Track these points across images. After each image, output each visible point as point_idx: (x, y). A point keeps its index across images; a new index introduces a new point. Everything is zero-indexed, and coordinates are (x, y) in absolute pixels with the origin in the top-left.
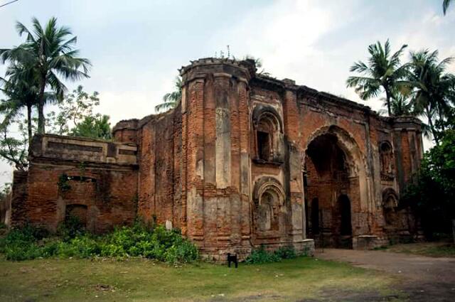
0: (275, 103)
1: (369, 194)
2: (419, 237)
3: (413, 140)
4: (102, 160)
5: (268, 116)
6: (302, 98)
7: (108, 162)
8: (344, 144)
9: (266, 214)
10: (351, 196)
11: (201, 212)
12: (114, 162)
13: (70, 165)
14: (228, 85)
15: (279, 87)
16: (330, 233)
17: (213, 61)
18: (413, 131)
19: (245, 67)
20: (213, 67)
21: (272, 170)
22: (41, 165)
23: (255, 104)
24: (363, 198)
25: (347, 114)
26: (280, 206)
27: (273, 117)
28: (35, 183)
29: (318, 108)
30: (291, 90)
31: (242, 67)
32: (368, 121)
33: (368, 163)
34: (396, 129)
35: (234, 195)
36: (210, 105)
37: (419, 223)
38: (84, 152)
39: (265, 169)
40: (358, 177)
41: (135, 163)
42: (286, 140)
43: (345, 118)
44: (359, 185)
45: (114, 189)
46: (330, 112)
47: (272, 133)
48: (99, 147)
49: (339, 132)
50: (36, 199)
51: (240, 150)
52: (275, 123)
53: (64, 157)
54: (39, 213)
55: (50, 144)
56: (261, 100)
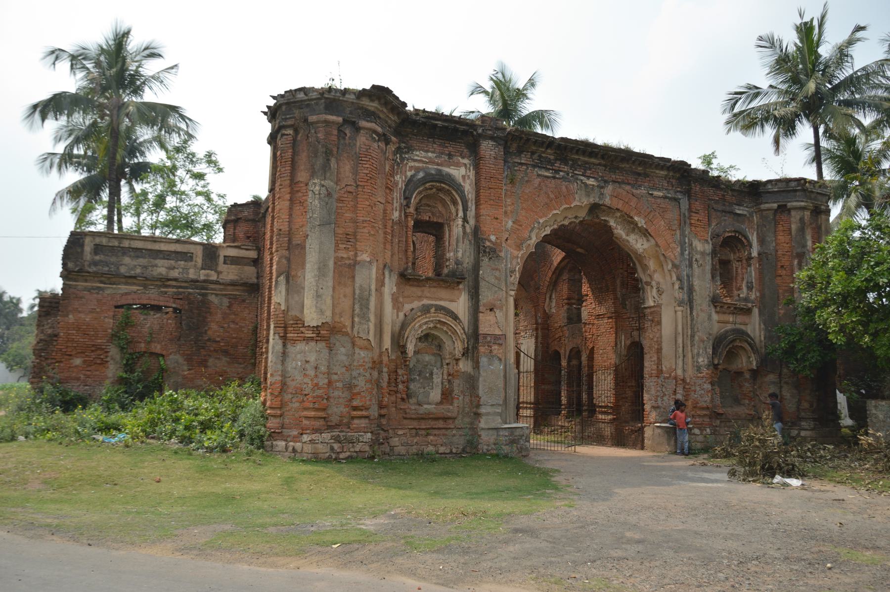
0: (458, 165)
1: (680, 341)
2: (803, 433)
3: (802, 230)
4: (192, 275)
5: (440, 190)
6: (520, 152)
7: (202, 278)
8: (628, 241)
9: (431, 374)
10: (646, 343)
11: (280, 367)
12: (214, 277)
13: (134, 284)
14: (334, 138)
15: (465, 133)
16: (610, 417)
17: (306, 94)
18: (803, 208)
19: (372, 101)
20: (308, 106)
21: (443, 293)
22: (81, 284)
23: (411, 168)
24: (667, 349)
25: (631, 179)
26: (457, 360)
27: (449, 193)
28: (71, 316)
29: (557, 171)
30: (492, 138)
32: (688, 193)
33: (678, 279)
34: (763, 206)
35: (338, 337)
37: (805, 405)
38: (160, 262)
39: (427, 291)
41: (255, 281)
42: (477, 238)
43: (628, 188)
44: (659, 323)
45: (214, 326)
46: (588, 177)
47: (450, 220)
48: (186, 253)
49: (612, 217)
50: (73, 340)
51: (356, 255)
52: (455, 203)
53: (123, 270)
54: (76, 366)
55: (98, 249)
56: (423, 159)
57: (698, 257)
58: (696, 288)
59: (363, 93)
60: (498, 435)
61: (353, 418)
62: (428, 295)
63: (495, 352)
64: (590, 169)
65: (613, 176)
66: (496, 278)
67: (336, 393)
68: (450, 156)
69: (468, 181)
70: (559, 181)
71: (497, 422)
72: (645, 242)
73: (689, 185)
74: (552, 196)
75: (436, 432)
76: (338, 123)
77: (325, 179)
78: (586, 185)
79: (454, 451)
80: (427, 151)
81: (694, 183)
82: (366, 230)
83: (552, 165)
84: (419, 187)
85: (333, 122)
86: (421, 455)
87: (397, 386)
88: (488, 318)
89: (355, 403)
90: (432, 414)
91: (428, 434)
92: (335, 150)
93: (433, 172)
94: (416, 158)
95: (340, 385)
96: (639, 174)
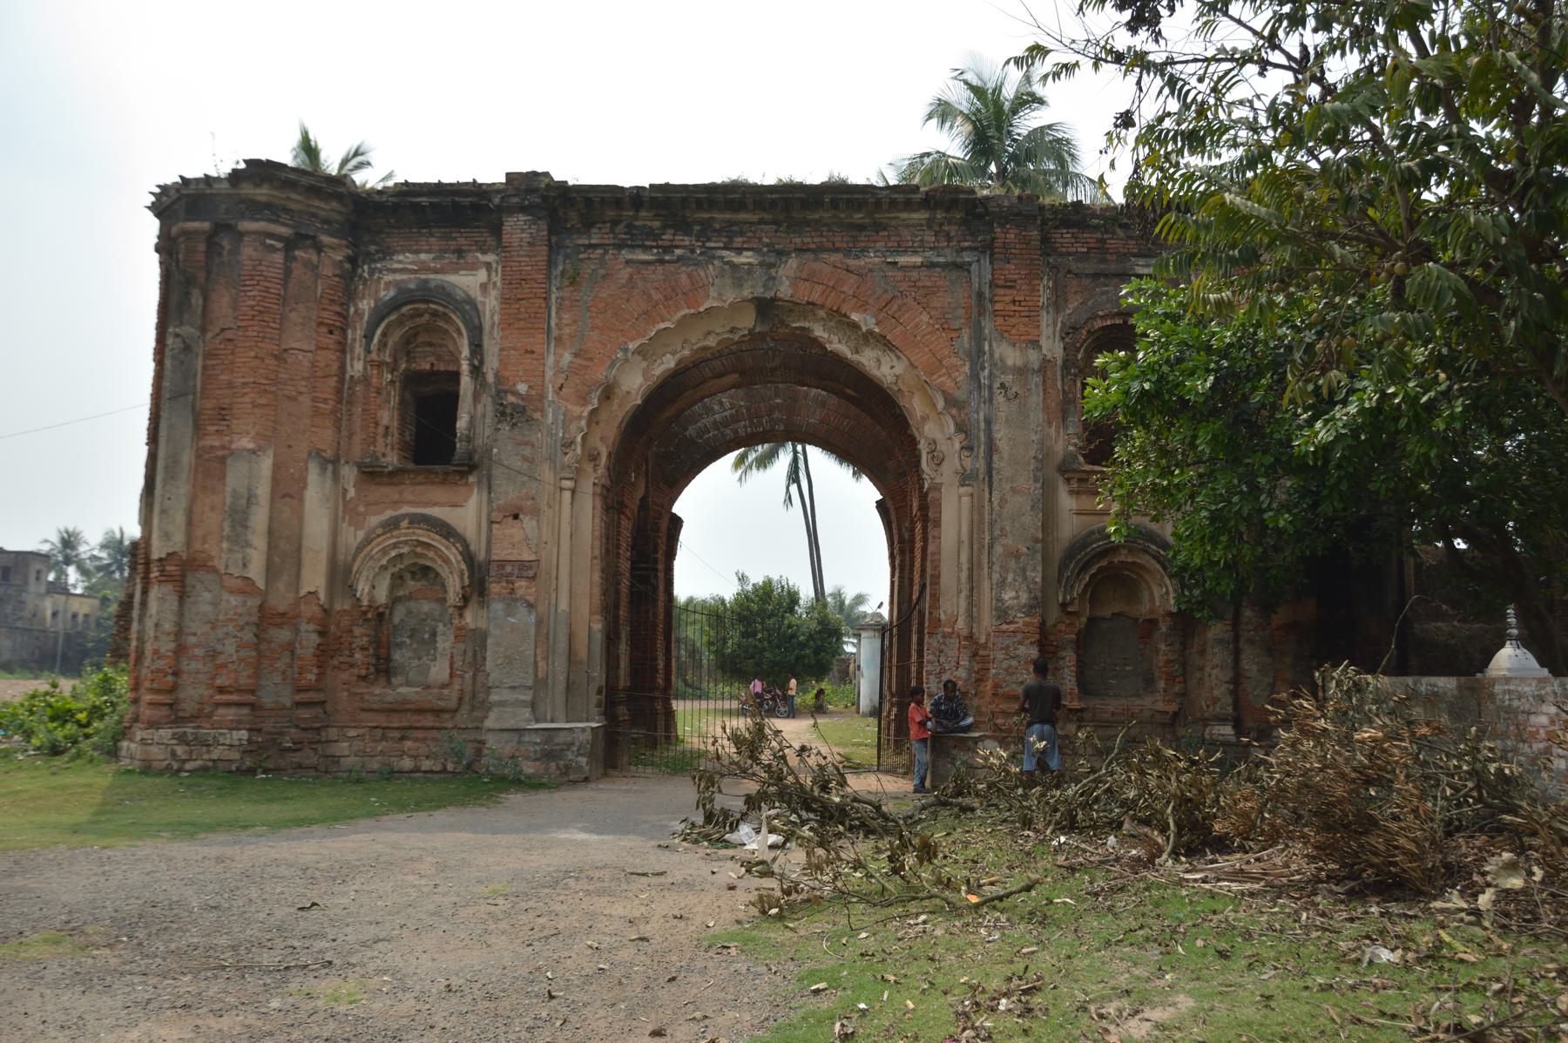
0: (473, 267)
5: (435, 314)
9: (434, 634)
14: (201, 257)
21: (438, 493)
23: (388, 284)
29: (668, 249)
30: (522, 209)
31: (247, 190)
32: (988, 248)
35: (201, 574)
43: (836, 258)
46: (739, 251)
49: (817, 320)
56: (405, 266)
57: (1008, 379)
58: (1002, 445)
59: (235, 175)
60: (519, 742)
61: (218, 705)
62: (411, 498)
63: (520, 592)
64: (742, 234)
65: (798, 240)
66: (525, 458)
67: (193, 665)
68: (460, 253)
69: (494, 293)
70: (672, 268)
71: (523, 718)
72: (895, 362)
73: (992, 231)
74: (656, 296)
75: (420, 734)
76: (204, 232)
77: (181, 324)
78: (734, 267)
79: (450, 767)
80: (417, 252)
81: (1002, 226)
82: (247, 399)
83: (657, 237)
84: (388, 314)
85: (196, 232)
86: (392, 774)
87: (351, 656)
89: (219, 682)
90: (410, 702)
91: (403, 738)
92: (201, 276)
93: (412, 286)
94: (396, 266)
95: (199, 652)
96: (861, 228)
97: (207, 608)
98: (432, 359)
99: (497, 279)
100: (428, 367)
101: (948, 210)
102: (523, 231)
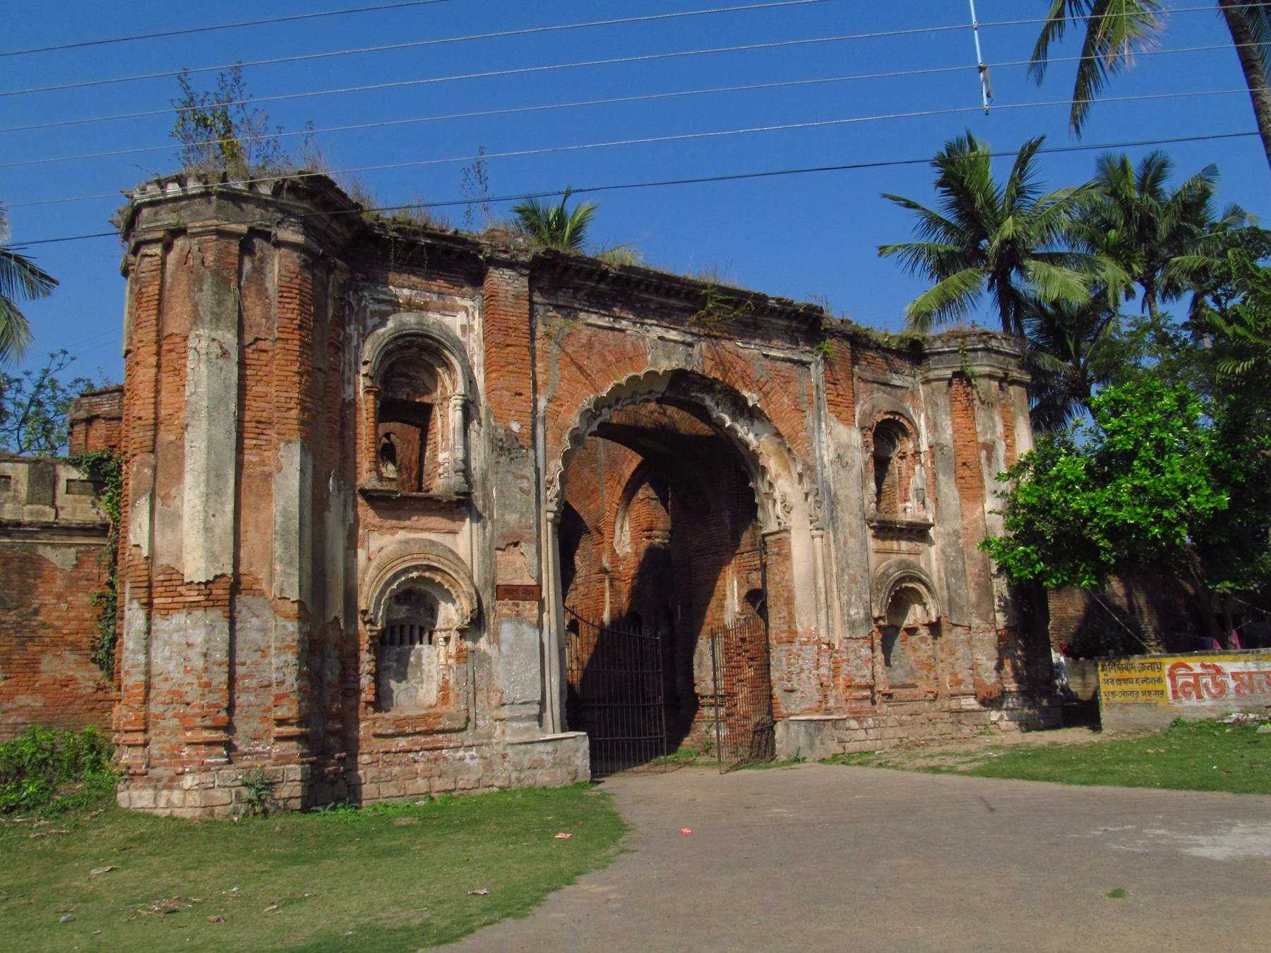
24: (802, 597)
36: (174, 325)
40: (787, 530)
74: (610, 358)
88: (511, 558)
94: (381, 296)
97: (256, 636)
98: (408, 390)
99: (477, 323)
100: (405, 397)
101: (800, 322)
102: (508, 284)
